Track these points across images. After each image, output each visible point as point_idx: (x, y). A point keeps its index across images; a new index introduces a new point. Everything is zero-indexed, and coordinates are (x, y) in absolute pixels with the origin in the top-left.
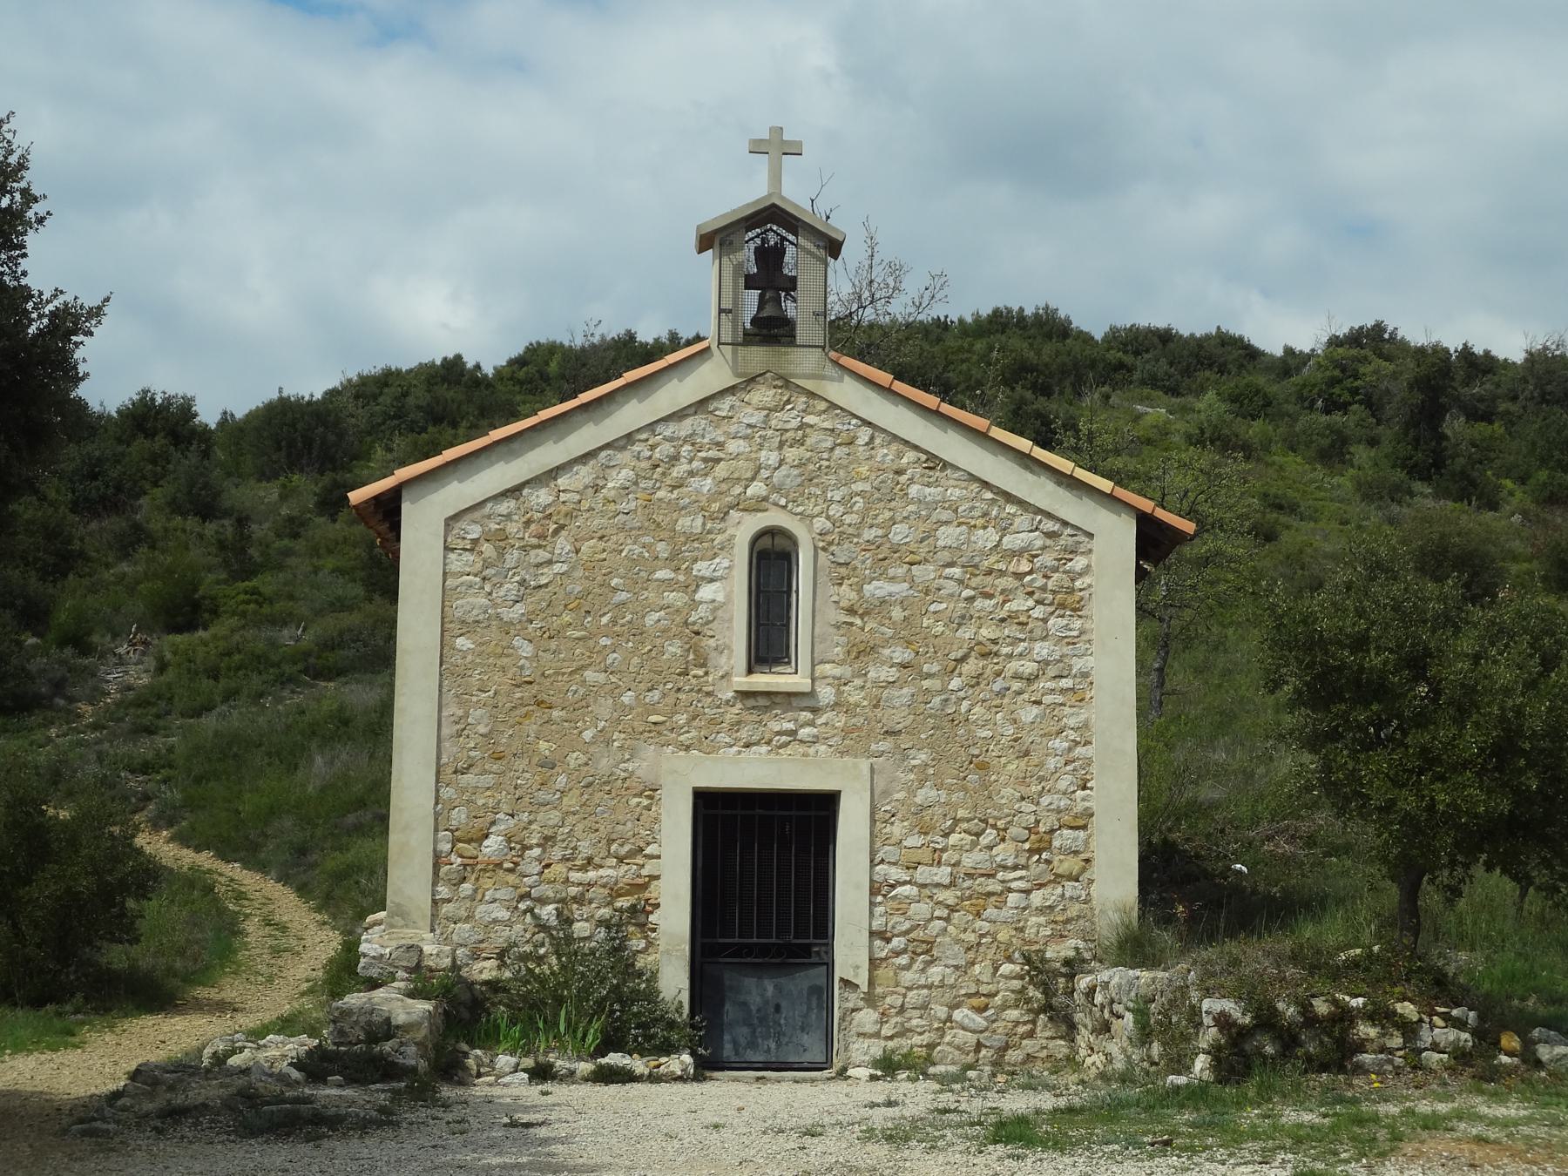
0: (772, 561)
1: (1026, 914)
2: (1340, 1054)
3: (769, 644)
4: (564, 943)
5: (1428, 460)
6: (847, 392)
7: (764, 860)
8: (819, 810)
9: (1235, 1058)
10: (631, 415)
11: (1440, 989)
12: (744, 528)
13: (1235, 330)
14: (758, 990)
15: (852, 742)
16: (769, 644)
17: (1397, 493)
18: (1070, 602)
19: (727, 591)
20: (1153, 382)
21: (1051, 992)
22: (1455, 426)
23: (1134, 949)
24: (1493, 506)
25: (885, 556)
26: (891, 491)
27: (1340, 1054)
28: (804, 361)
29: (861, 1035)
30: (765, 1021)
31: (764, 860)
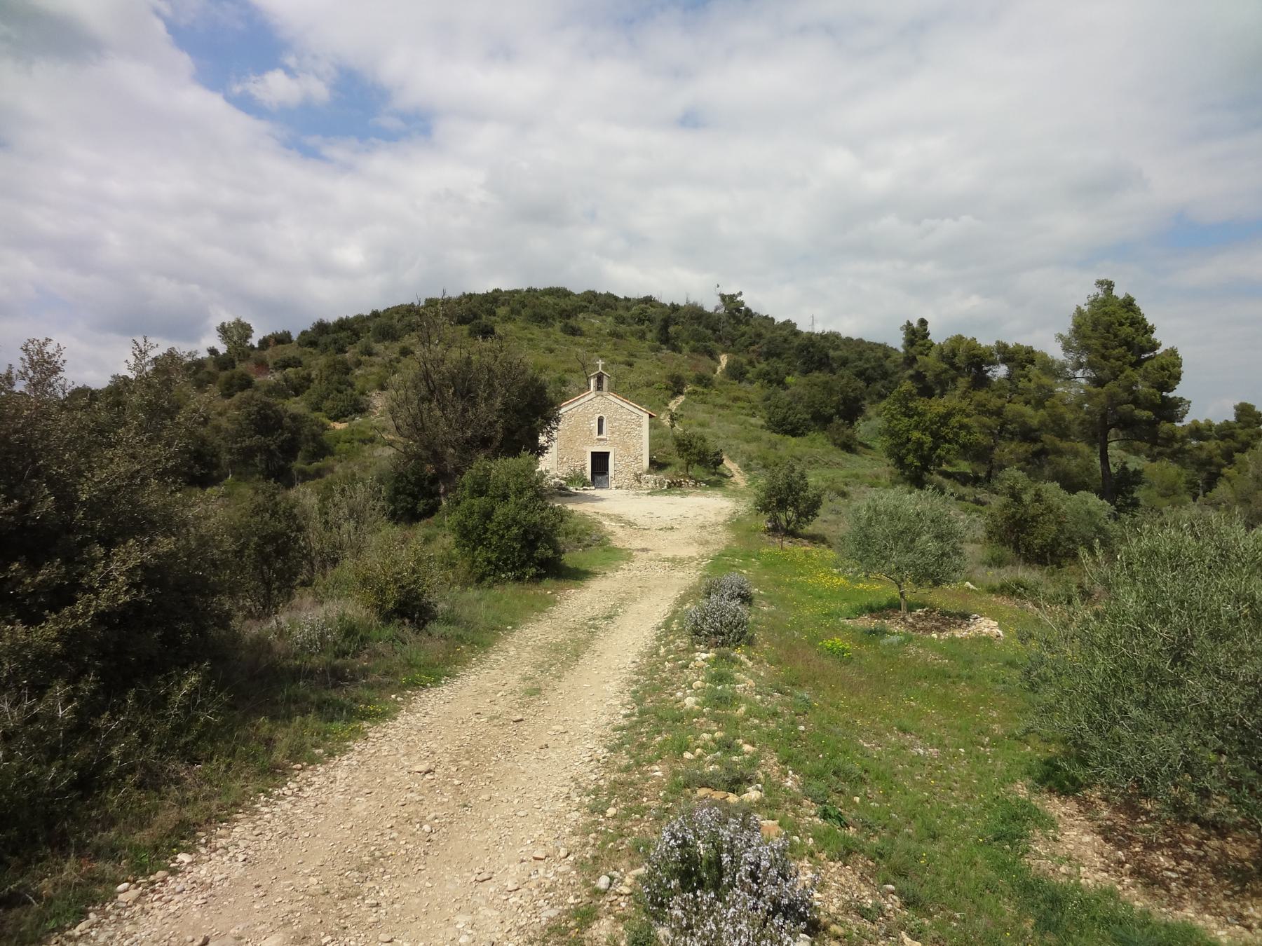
0: (601, 420)
1: (634, 467)
2: (680, 485)
3: (600, 432)
4: (574, 471)
5: (666, 339)
6: (610, 397)
7: (600, 461)
8: (606, 455)
9: (669, 486)
10: (582, 401)
11: (691, 478)
12: (597, 416)
13: (612, 292)
14: (599, 478)
15: (611, 445)
16: (600, 432)
17: (658, 350)
18: (640, 426)
19: (595, 425)
20: (594, 312)
21: (638, 478)
22: (672, 329)
23: (648, 472)
24: (680, 352)
25: (616, 420)
26: (616, 411)
27: (680, 485)
28: (605, 393)
29: (613, 484)
30: (600, 482)
31: (600, 461)
